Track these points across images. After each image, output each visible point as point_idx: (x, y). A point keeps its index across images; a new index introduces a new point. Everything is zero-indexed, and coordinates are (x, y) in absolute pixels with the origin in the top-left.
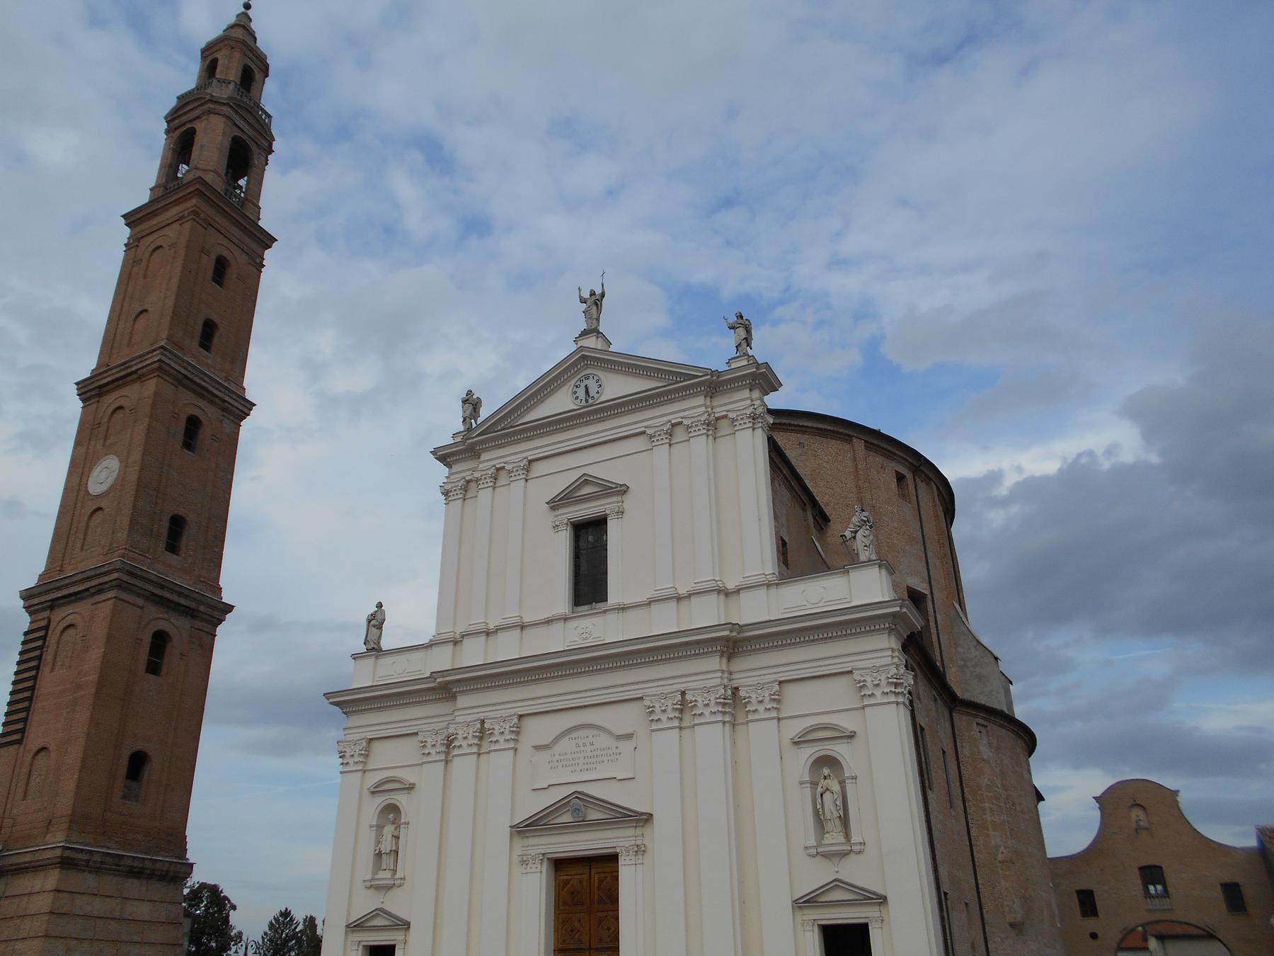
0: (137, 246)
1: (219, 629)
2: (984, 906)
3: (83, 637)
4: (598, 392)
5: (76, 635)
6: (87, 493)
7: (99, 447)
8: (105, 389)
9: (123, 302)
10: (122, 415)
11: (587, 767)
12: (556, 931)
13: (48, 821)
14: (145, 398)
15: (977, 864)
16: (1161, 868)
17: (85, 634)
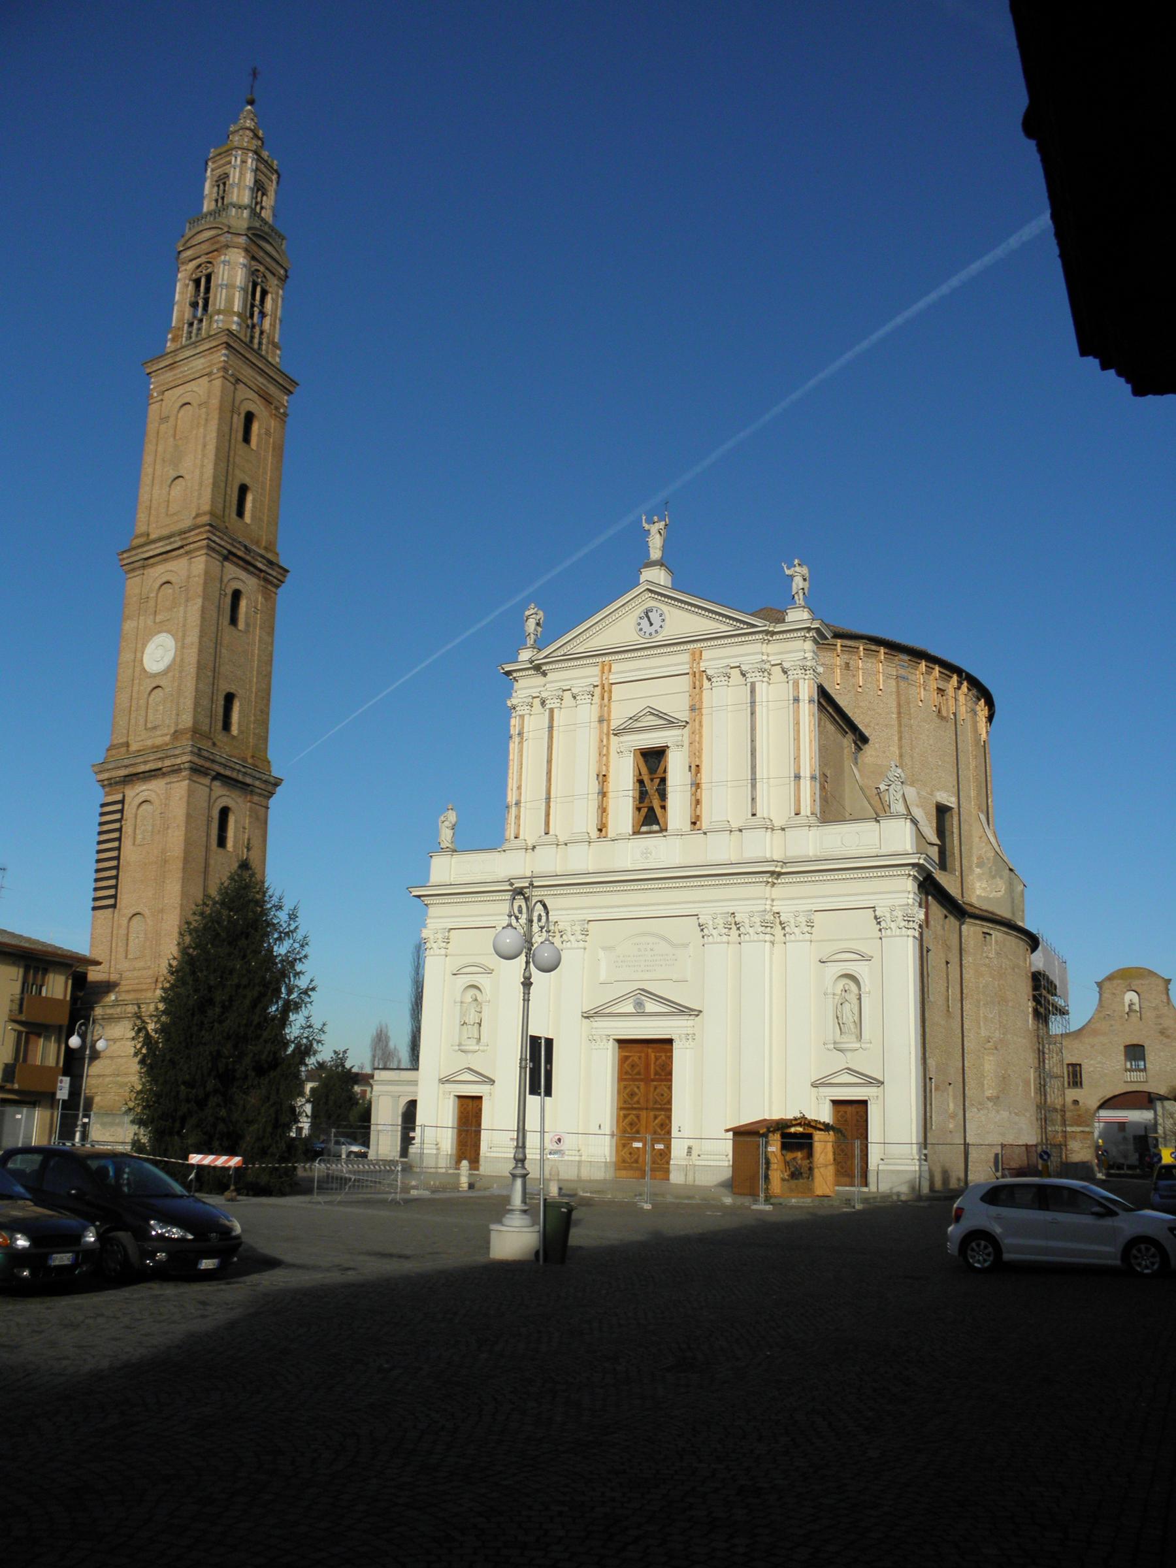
0: (162, 400)
1: (272, 802)
2: (966, 1084)
3: (161, 814)
4: (661, 627)
5: (154, 812)
6: (144, 670)
7: (150, 622)
8: (152, 561)
9: (155, 464)
10: (170, 591)
11: (649, 968)
12: (619, 1092)
13: (155, 979)
14: (195, 576)
15: (965, 1051)
16: (1143, 1046)
17: (163, 811)
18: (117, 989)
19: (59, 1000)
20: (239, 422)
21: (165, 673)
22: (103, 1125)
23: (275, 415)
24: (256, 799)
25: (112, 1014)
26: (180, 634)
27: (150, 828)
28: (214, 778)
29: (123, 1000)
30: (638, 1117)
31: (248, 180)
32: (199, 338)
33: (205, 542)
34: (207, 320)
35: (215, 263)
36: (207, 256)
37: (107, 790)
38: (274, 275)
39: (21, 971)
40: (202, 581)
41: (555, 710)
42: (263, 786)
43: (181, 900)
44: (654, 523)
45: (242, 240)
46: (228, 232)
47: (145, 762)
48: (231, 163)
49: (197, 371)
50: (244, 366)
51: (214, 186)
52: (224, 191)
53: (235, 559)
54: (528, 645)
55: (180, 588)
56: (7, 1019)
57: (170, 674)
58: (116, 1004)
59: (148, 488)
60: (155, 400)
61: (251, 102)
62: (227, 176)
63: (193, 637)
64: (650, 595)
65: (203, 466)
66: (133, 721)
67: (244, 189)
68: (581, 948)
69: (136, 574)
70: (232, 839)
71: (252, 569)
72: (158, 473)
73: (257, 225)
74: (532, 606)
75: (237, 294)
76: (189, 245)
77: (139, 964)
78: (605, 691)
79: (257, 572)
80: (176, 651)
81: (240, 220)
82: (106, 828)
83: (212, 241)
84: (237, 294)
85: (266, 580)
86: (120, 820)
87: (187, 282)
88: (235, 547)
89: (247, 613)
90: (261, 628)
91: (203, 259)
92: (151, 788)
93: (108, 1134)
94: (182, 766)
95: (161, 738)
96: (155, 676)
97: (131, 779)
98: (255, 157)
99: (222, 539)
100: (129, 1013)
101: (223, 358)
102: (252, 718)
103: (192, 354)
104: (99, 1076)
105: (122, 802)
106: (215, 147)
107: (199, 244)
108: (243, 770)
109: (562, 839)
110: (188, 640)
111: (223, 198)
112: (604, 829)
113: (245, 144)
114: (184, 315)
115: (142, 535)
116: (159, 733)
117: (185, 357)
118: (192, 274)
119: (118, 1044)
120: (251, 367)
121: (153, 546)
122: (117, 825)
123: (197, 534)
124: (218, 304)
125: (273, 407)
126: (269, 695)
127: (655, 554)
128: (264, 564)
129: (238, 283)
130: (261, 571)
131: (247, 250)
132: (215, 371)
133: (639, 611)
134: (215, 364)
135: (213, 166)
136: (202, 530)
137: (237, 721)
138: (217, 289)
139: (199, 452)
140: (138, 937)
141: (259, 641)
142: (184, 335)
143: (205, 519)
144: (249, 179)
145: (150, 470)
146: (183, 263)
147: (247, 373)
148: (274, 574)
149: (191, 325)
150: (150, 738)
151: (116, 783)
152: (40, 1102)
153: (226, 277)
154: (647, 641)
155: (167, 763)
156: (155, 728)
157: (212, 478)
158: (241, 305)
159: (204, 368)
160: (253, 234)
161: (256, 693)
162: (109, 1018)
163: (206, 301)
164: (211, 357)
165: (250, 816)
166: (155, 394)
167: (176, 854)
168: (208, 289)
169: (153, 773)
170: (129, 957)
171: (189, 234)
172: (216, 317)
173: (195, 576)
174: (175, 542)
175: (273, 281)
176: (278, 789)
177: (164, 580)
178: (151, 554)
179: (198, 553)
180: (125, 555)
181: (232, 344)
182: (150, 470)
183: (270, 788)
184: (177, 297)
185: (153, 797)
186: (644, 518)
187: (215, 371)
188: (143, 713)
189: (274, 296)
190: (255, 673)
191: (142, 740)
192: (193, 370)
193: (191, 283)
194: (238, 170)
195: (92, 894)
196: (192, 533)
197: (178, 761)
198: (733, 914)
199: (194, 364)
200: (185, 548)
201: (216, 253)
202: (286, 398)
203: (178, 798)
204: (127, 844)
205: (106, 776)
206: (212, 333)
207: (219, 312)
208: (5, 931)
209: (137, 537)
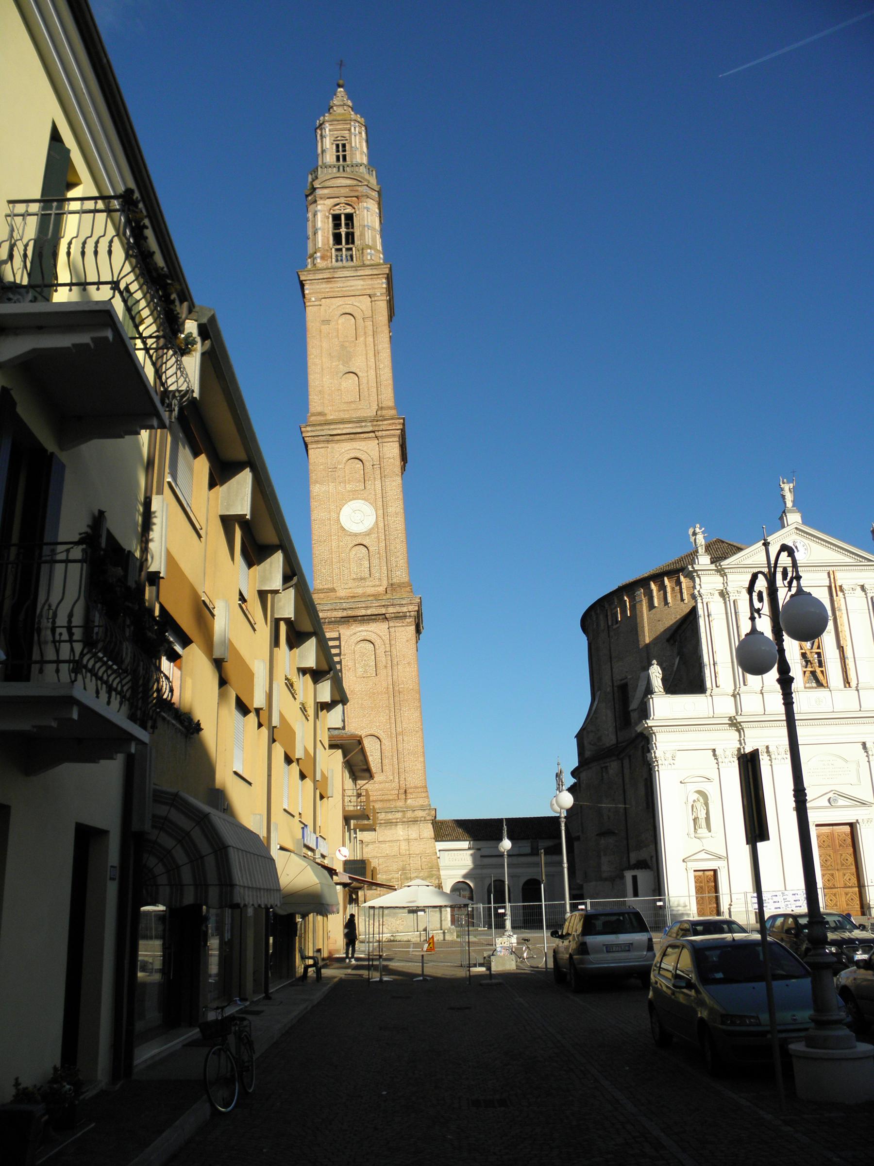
8: (338, 437)
14: (389, 458)
21: (368, 534)
30: (832, 875)
36: (346, 199)
46: (367, 185)
47: (367, 608)
49: (358, 290)
51: (333, 144)
57: (373, 536)
64: (796, 531)
69: (319, 446)
83: (351, 188)
87: (327, 214)
91: (343, 200)
94: (408, 614)
95: (376, 586)
96: (356, 535)
100: (382, 820)
103: (352, 275)
107: (337, 187)
118: (330, 209)
121: (341, 426)
123: (390, 424)
150: (358, 587)
153: (369, 221)
155: (391, 610)
164: (370, 282)
166: (313, 299)
167: (411, 687)
169: (373, 617)
174: (365, 426)
178: (339, 432)
185: (372, 637)
187: (379, 294)
191: (350, 588)
192: (353, 288)
193: (330, 216)
196: (385, 422)
197: (405, 609)
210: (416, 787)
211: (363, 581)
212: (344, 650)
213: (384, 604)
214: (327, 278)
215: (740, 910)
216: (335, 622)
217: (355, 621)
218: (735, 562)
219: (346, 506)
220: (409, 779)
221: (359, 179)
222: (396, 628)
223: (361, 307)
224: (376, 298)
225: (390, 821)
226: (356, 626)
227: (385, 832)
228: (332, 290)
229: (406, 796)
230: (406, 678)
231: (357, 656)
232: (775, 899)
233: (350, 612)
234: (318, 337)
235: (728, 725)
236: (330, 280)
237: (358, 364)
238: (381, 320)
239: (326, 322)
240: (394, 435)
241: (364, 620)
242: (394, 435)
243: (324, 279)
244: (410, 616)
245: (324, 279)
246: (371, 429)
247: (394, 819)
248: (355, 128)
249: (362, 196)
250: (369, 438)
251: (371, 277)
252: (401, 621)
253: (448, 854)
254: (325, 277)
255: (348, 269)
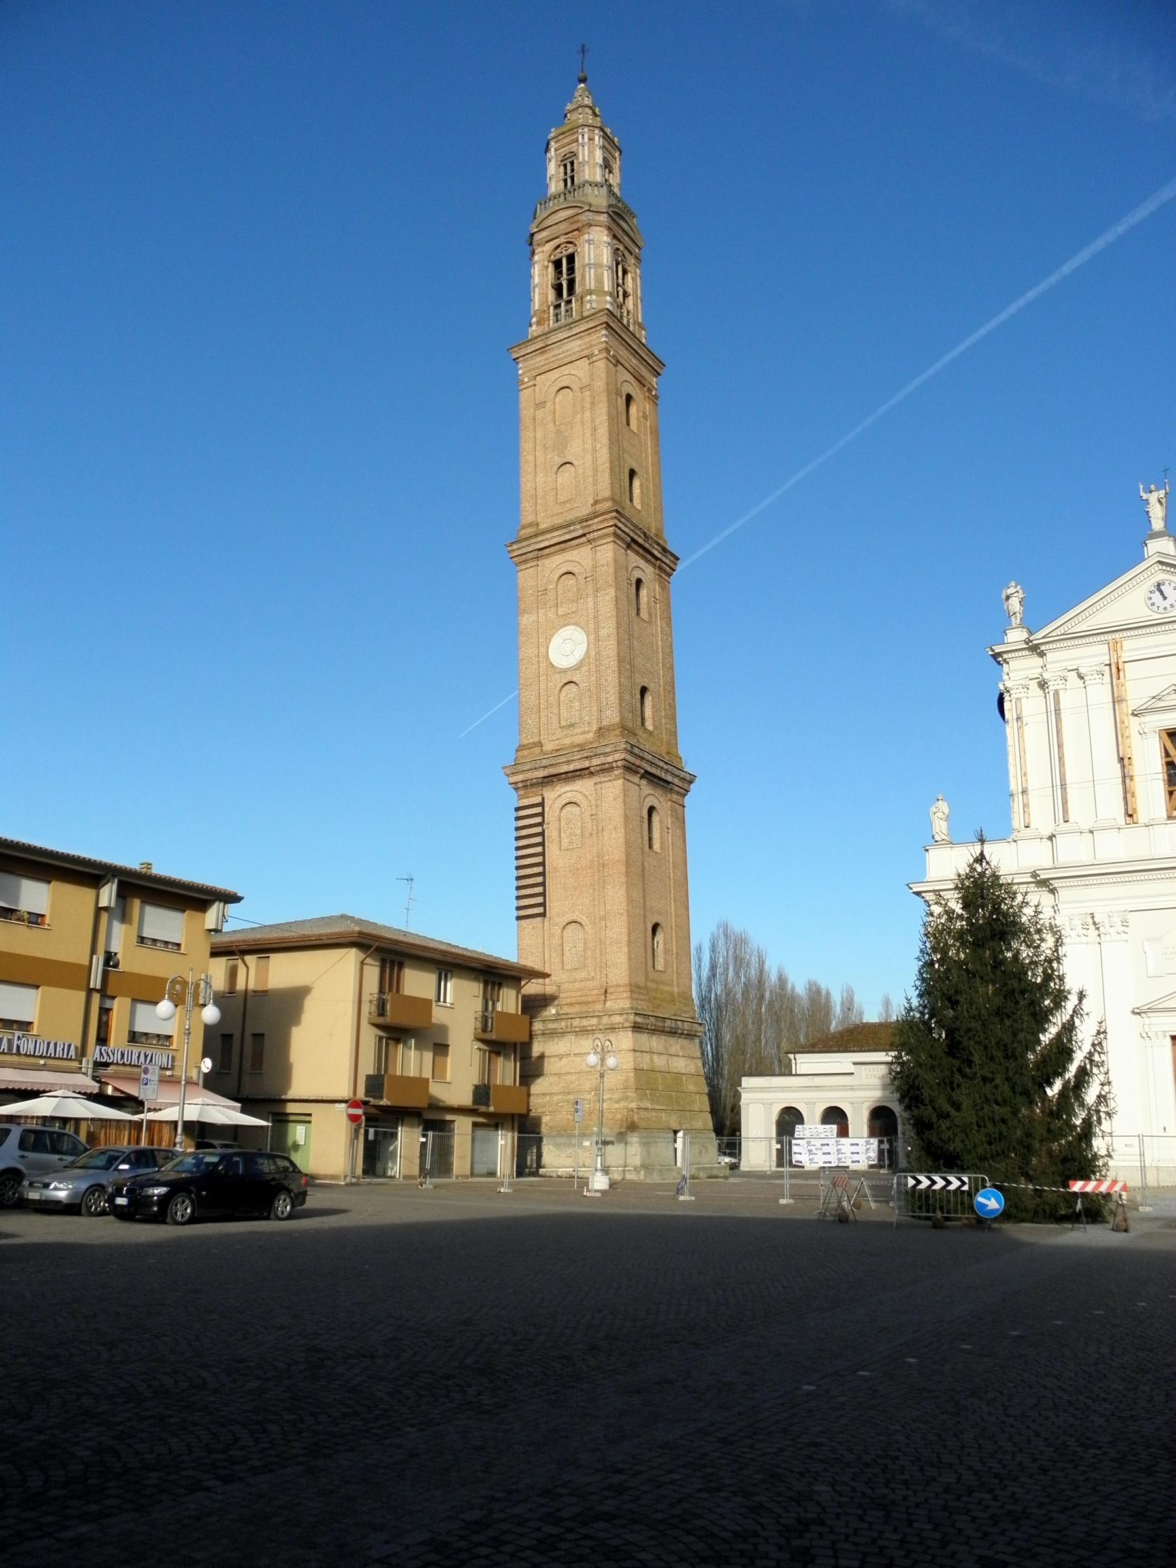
1: (688, 800)
3: (591, 816)
14: (603, 565)
18: (556, 1002)
19: (512, 1014)
20: (622, 402)
21: (578, 667)
22: (557, 1145)
23: (649, 397)
24: (675, 797)
25: (555, 1029)
26: (592, 626)
27: (578, 831)
28: (642, 777)
29: (566, 1014)
31: (597, 157)
32: (571, 320)
33: (612, 529)
34: (577, 301)
35: (577, 243)
37: (521, 792)
38: (631, 254)
39: (481, 986)
40: (612, 570)
41: (1061, 692)
42: (680, 784)
43: (628, 906)
44: (1151, 492)
45: (603, 218)
46: (589, 210)
47: (568, 762)
48: (577, 141)
49: (574, 353)
50: (621, 347)
51: (559, 166)
52: (572, 170)
53: (636, 547)
54: (1014, 625)
55: (585, 578)
56: (473, 1038)
57: (585, 668)
58: (558, 1018)
59: (530, 477)
60: (525, 386)
61: (583, 80)
62: (574, 154)
63: (609, 628)
64: (1160, 567)
65: (595, 450)
66: (543, 720)
67: (594, 167)
68: (1123, 941)
69: (529, 565)
70: (659, 841)
71: (649, 556)
72: (540, 460)
73: (614, 202)
74: (1013, 583)
75: (605, 273)
76: (541, 227)
77: (583, 974)
78: (1116, 670)
79: (653, 560)
80: (588, 644)
81: (600, 199)
82: (524, 832)
83: (572, 220)
84: (605, 273)
85: (660, 568)
86: (541, 824)
87: (546, 263)
88: (636, 534)
89: (648, 603)
90: (661, 619)
91: (562, 239)
92: (576, 789)
93: (563, 1156)
94: (614, 765)
95: (584, 734)
96: (565, 671)
97: (550, 780)
98: (602, 134)
99: (626, 526)
100: (576, 1027)
101: (604, 339)
102: (663, 713)
104: (545, 1094)
105: (542, 804)
106: (557, 127)
107: (556, 224)
108: (665, 767)
109: (1086, 826)
110: (603, 632)
111: (572, 178)
112: (1134, 815)
113: (590, 121)
114: (547, 297)
115: (530, 525)
116: (576, 731)
117: (557, 340)
118: (550, 256)
119: (564, 1060)
120: (626, 348)
121: (549, 536)
122: (538, 830)
123: (601, 522)
124: (587, 283)
125: (645, 389)
126: (673, 688)
127: (1158, 524)
128: (660, 552)
129: (605, 262)
130: (657, 559)
131: (609, 229)
132: (596, 352)
133: (1150, 584)
134: (594, 345)
135: (557, 145)
136: (608, 516)
137: (651, 716)
138: (584, 271)
139: (588, 435)
140: (575, 947)
141: (661, 632)
142: (551, 318)
143: (608, 505)
144: (599, 156)
145: (530, 458)
146: (539, 245)
147: (624, 354)
148: (667, 561)
149: (558, 306)
150: (566, 736)
151: (532, 785)
152: (502, 1124)
153: (592, 257)
154: (1161, 616)
155: (596, 761)
156: (572, 725)
157: (608, 462)
158: (610, 284)
159: (582, 350)
160: (613, 212)
161: (664, 687)
162: (551, 1033)
163: (571, 283)
164: (587, 339)
165: (672, 816)
166: (526, 380)
167: (617, 858)
168: (571, 270)
169: (578, 773)
170: (566, 967)
171: (541, 215)
172: (588, 298)
173: (603, 565)
174: (574, 530)
175: (631, 260)
176: (692, 786)
177: (564, 570)
178: (547, 543)
179: (604, 541)
180: (515, 547)
181: (612, 325)
182: (530, 458)
183: (685, 786)
184: (536, 280)
185: (578, 798)
186: (1141, 487)
187: (596, 352)
188: (555, 711)
189: (633, 275)
190: (661, 665)
191: (558, 739)
193: (550, 264)
194: (586, 147)
195: (515, 903)
196: (596, 520)
197: (610, 759)
198: (1092, 914)
199: (569, 346)
200: (588, 536)
201: (576, 232)
202: (655, 379)
203: (612, 798)
204: (552, 850)
205: (520, 777)
206: (586, 314)
207: (590, 292)
208: (433, 939)
209: (524, 527)
210: (618, 986)
211: (571, 728)
212: (548, 818)
213: (585, 755)
214: (539, 349)
215: (1132, 1164)
216: (538, 783)
217: (559, 780)
218: (1061, 630)
219: (556, 635)
220: (611, 975)
221: (579, 205)
222: (603, 784)
223: (578, 375)
224: (594, 359)
225: (585, 1029)
226: (561, 787)
227: (582, 1042)
228: (547, 361)
229: (605, 997)
230: (611, 847)
231: (562, 824)
232: (826, 1149)
233: (552, 770)
234: (531, 426)
235: (1033, 885)
236: (543, 350)
237: (574, 451)
238: (599, 386)
239: (542, 405)
240: (607, 535)
241: (568, 778)
242: (607, 535)
243: (537, 350)
244: (617, 767)
245: (537, 350)
246: (580, 532)
247: (589, 1026)
248: (583, 135)
249: (583, 226)
250: (582, 544)
251: (587, 332)
252: (609, 774)
253: (873, 1069)
254: (537, 347)
255: (562, 330)
